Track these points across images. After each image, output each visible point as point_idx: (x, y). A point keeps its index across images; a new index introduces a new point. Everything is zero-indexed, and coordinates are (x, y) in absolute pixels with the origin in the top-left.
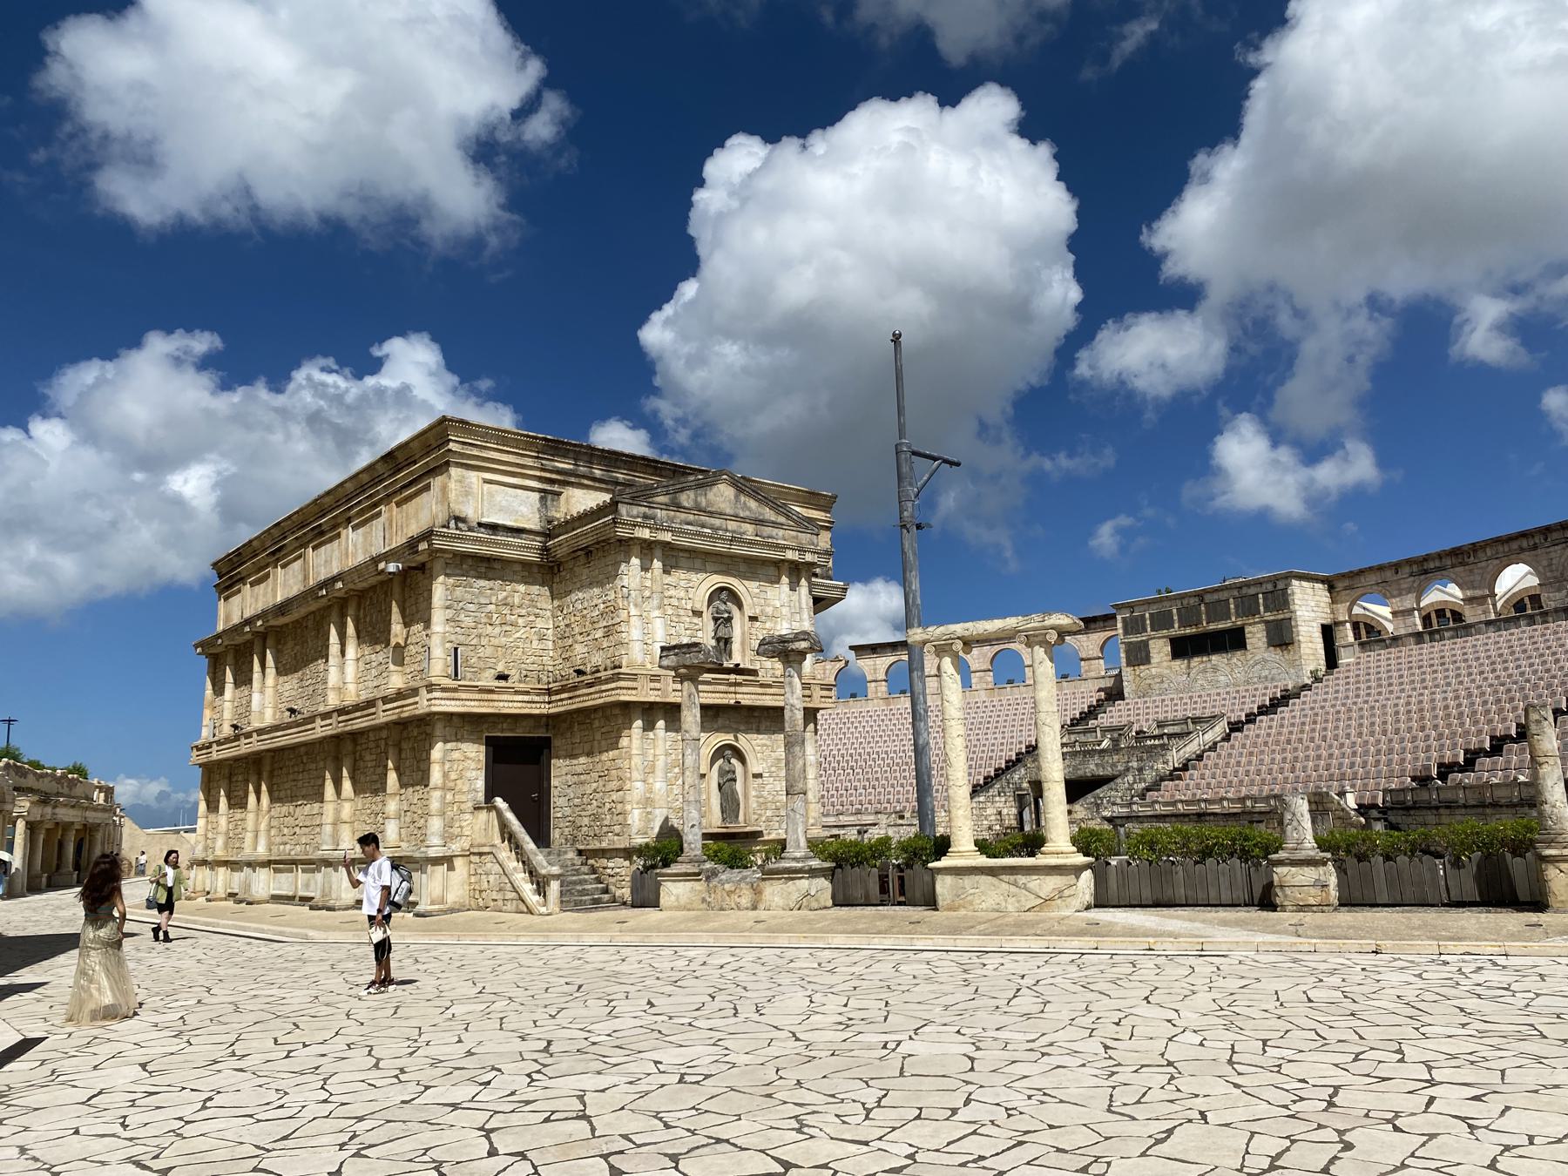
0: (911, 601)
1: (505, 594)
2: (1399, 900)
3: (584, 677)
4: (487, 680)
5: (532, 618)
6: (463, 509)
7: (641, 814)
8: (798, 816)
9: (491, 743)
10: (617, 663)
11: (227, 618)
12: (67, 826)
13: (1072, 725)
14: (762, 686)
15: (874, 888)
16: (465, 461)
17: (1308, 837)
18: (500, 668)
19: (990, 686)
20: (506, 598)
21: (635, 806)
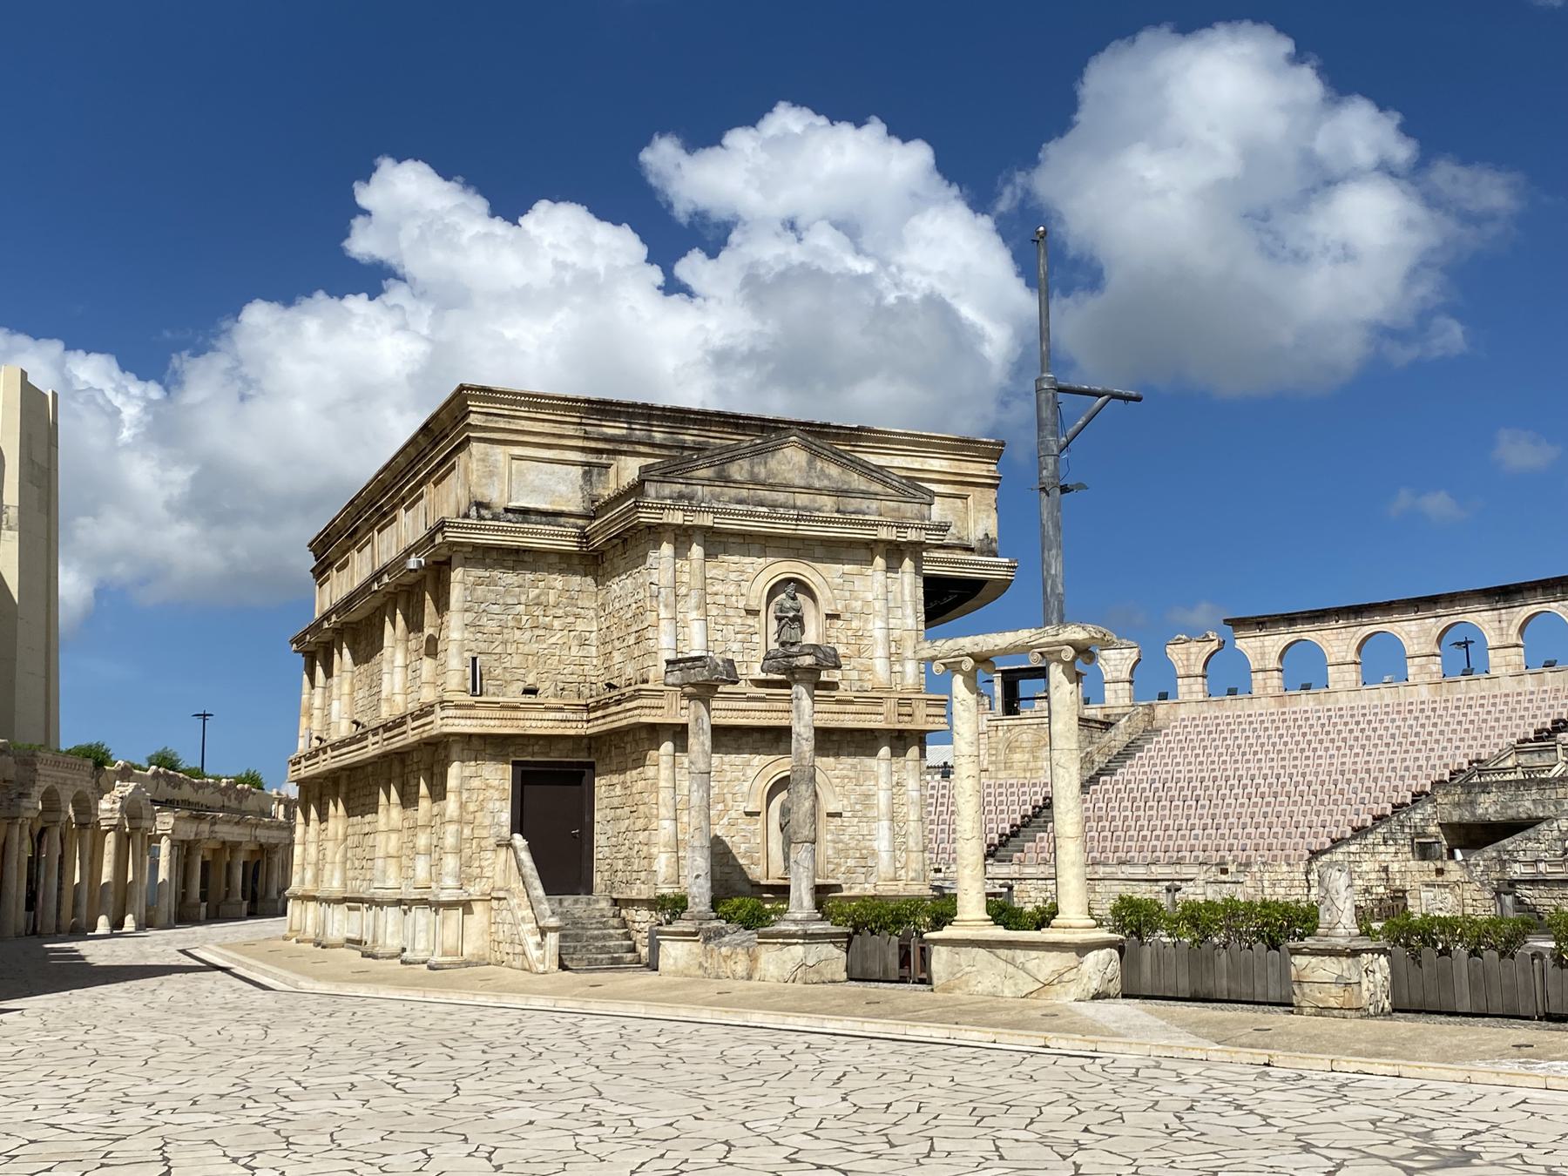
0: (1049, 589)
1: (537, 591)
2: (1483, 1010)
3: (614, 694)
4: (514, 695)
5: (571, 619)
6: (486, 492)
7: (668, 859)
8: (801, 870)
9: (515, 764)
10: (645, 677)
11: (322, 606)
12: (234, 847)
13: (1537, 739)
14: (839, 702)
15: (894, 961)
17: (1343, 920)
18: (531, 680)
19: (1435, 679)
20: (538, 596)
21: (662, 849)
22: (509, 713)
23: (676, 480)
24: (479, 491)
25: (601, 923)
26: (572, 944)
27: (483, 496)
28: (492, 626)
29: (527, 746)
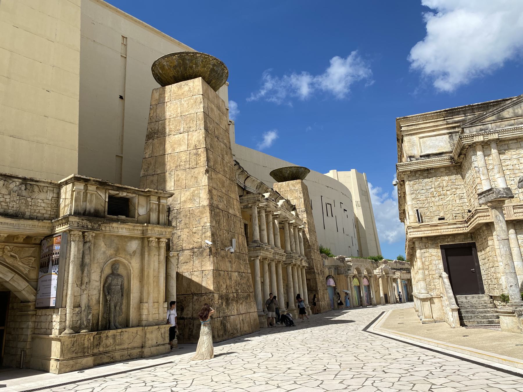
1: (438, 182)
4: (436, 221)
5: (454, 190)
9: (442, 247)
16: (409, 133)
18: (442, 215)
20: (439, 184)
22: (434, 228)
23: (478, 124)
24: (409, 152)
25: (484, 306)
26: (470, 315)
27: (411, 154)
28: (423, 198)
29: (445, 239)
